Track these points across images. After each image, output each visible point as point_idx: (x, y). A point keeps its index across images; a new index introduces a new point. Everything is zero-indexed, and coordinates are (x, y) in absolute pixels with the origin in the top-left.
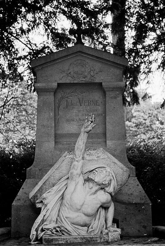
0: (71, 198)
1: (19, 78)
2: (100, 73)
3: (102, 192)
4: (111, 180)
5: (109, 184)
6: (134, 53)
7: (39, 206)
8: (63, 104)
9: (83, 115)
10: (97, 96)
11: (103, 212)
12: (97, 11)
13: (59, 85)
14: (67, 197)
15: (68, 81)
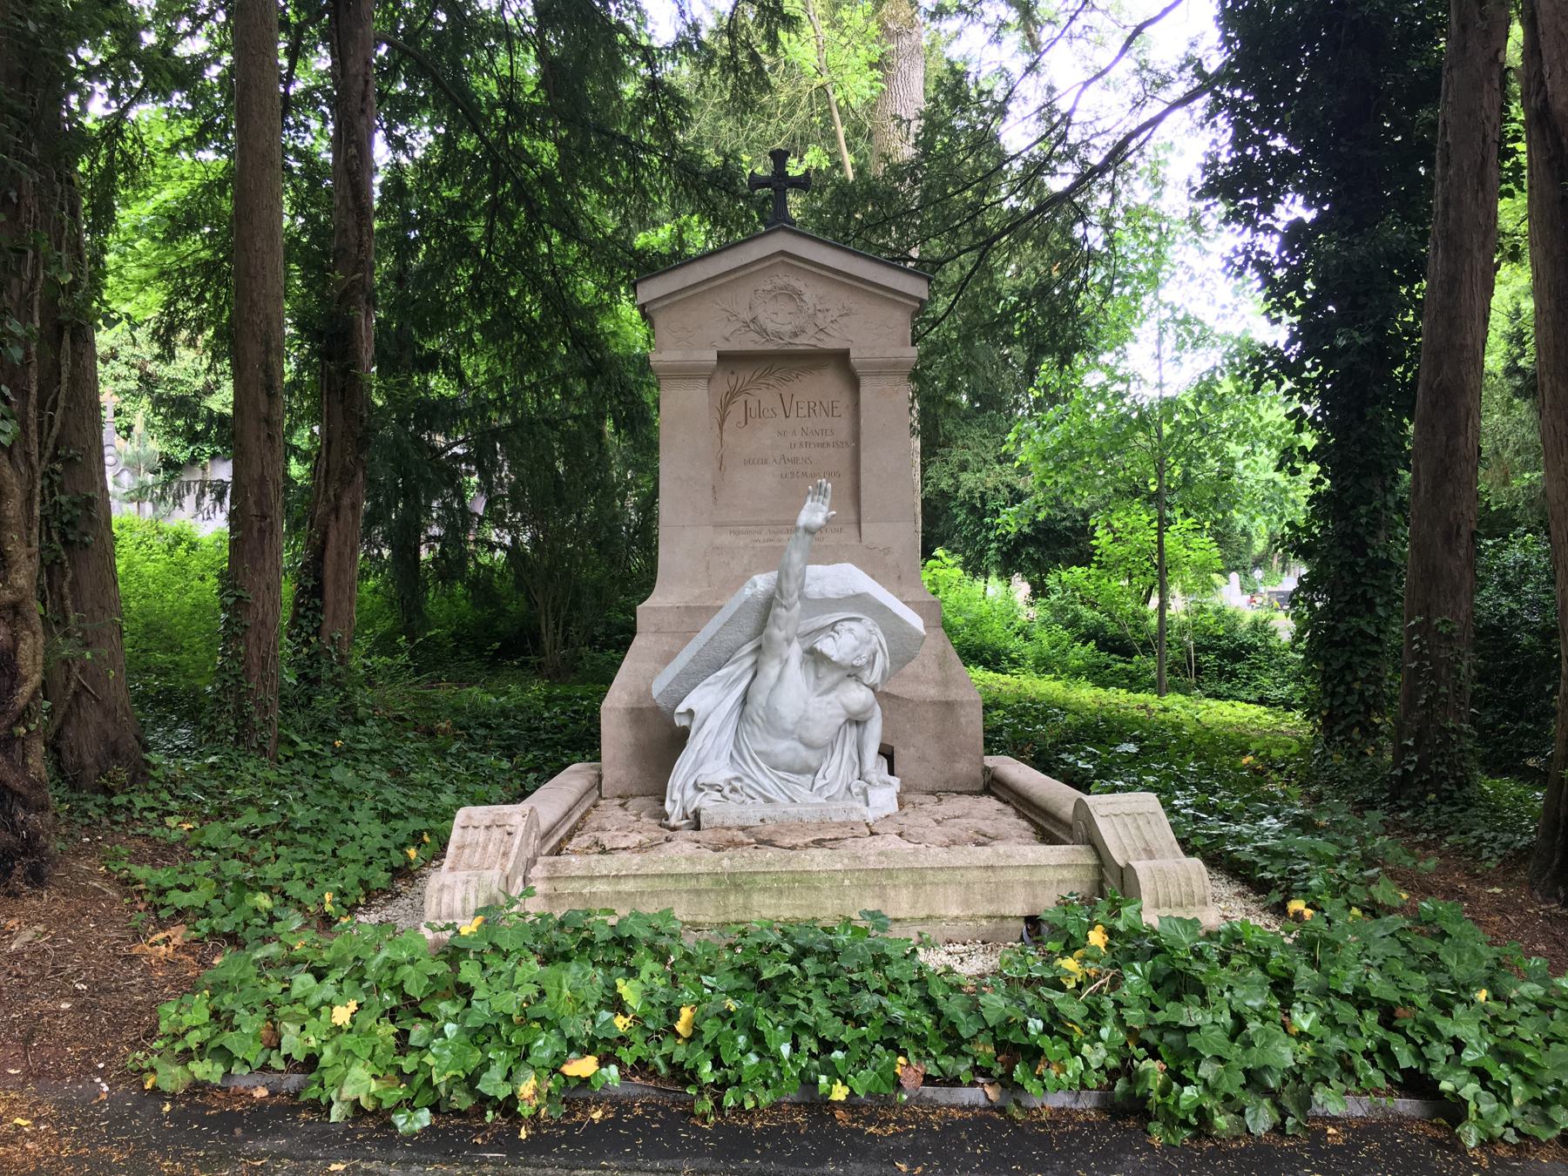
0: (768, 702)
1: (556, 240)
2: (845, 320)
3: (853, 685)
4: (874, 655)
5: (871, 663)
6: (423, 137)
7: (680, 722)
8: (736, 411)
9: (793, 446)
10: (827, 385)
11: (852, 733)
12: (1502, 47)
13: (722, 357)
14: (759, 699)
15: (751, 347)
